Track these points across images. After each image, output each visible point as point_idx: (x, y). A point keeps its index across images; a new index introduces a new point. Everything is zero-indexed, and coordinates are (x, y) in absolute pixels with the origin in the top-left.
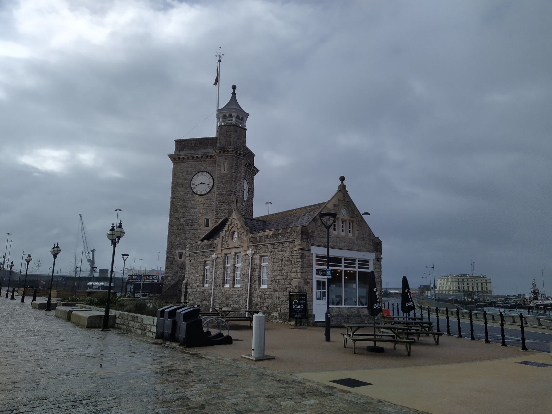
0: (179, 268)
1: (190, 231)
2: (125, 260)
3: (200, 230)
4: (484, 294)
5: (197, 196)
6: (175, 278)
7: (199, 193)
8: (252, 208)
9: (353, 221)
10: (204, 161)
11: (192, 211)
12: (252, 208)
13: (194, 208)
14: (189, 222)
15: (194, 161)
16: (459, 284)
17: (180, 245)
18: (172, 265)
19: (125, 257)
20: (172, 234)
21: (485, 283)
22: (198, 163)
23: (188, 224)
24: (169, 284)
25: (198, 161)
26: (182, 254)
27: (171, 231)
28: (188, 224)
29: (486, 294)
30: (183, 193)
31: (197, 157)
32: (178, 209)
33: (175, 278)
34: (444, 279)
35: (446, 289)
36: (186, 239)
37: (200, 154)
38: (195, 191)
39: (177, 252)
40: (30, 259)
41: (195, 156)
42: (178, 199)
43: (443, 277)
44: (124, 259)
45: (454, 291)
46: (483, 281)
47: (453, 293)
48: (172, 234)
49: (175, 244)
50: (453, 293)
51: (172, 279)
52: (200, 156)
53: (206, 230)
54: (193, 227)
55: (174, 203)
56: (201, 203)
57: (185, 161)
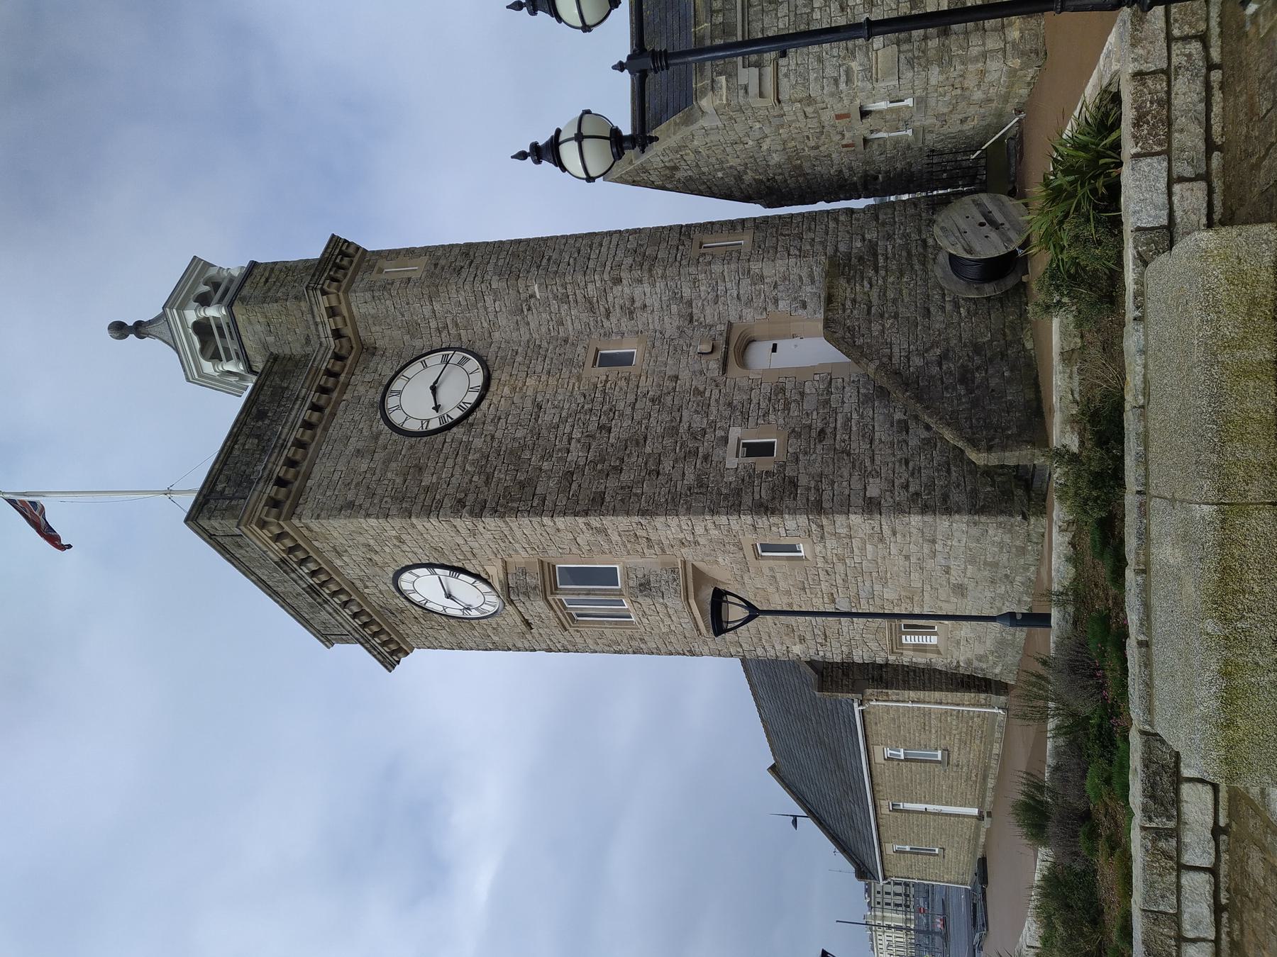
0: (819, 447)
1: (637, 417)
2: (754, 612)
3: (643, 378)
4: (912, 903)
5: (484, 405)
6: (873, 461)
7: (472, 398)
8: (597, 240)
9: (701, 244)
10: (343, 392)
11: (548, 417)
12: (597, 240)
13: (536, 410)
14: (593, 427)
15: (326, 429)
16: (888, 904)
17: (700, 455)
18: (803, 480)
19: (735, 613)
20: (639, 496)
21: (885, 896)
22: (340, 413)
23: (601, 428)
24: (906, 487)
25: (333, 415)
26: (745, 445)
27: (622, 500)
28: (601, 428)
29: (912, 899)
30: (450, 462)
31: (315, 408)
32: (521, 477)
33: (873, 461)
34: (879, 937)
35: (902, 940)
36: (673, 431)
37: (304, 391)
38: (456, 414)
39: (732, 462)
40: (579, 138)
41: (306, 414)
42: (471, 481)
43: (873, 944)
44: (746, 621)
45: (906, 919)
46: (880, 900)
47: (913, 922)
48: (639, 496)
49: (692, 477)
50: (913, 922)
51: (879, 474)
52: (313, 397)
53: (647, 355)
54: (621, 406)
55: (485, 501)
56: (521, 389)
57: (306, 463)
